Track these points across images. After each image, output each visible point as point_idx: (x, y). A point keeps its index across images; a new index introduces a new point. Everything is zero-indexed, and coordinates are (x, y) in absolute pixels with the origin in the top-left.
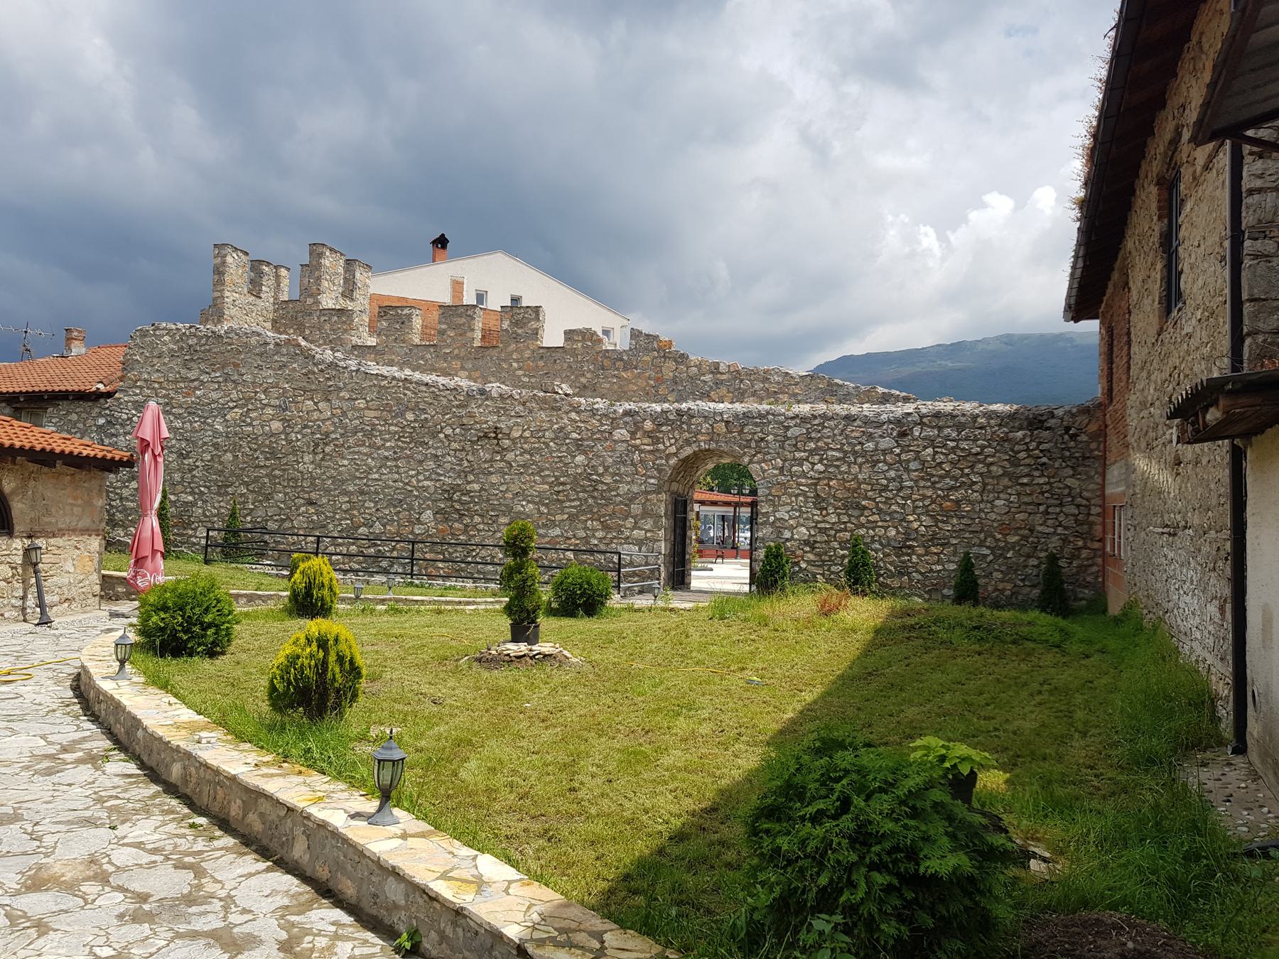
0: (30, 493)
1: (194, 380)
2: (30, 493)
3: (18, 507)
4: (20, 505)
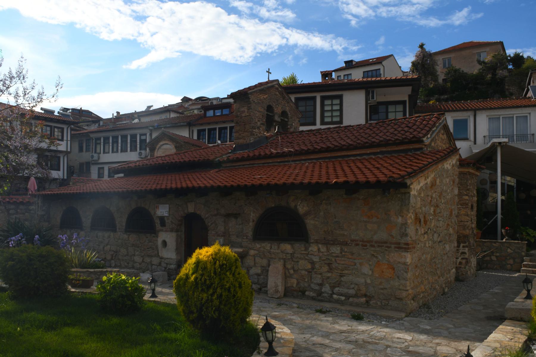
0: (322, 213)
2: (322, 213)
3: (310, 223)
4: (312, 222)
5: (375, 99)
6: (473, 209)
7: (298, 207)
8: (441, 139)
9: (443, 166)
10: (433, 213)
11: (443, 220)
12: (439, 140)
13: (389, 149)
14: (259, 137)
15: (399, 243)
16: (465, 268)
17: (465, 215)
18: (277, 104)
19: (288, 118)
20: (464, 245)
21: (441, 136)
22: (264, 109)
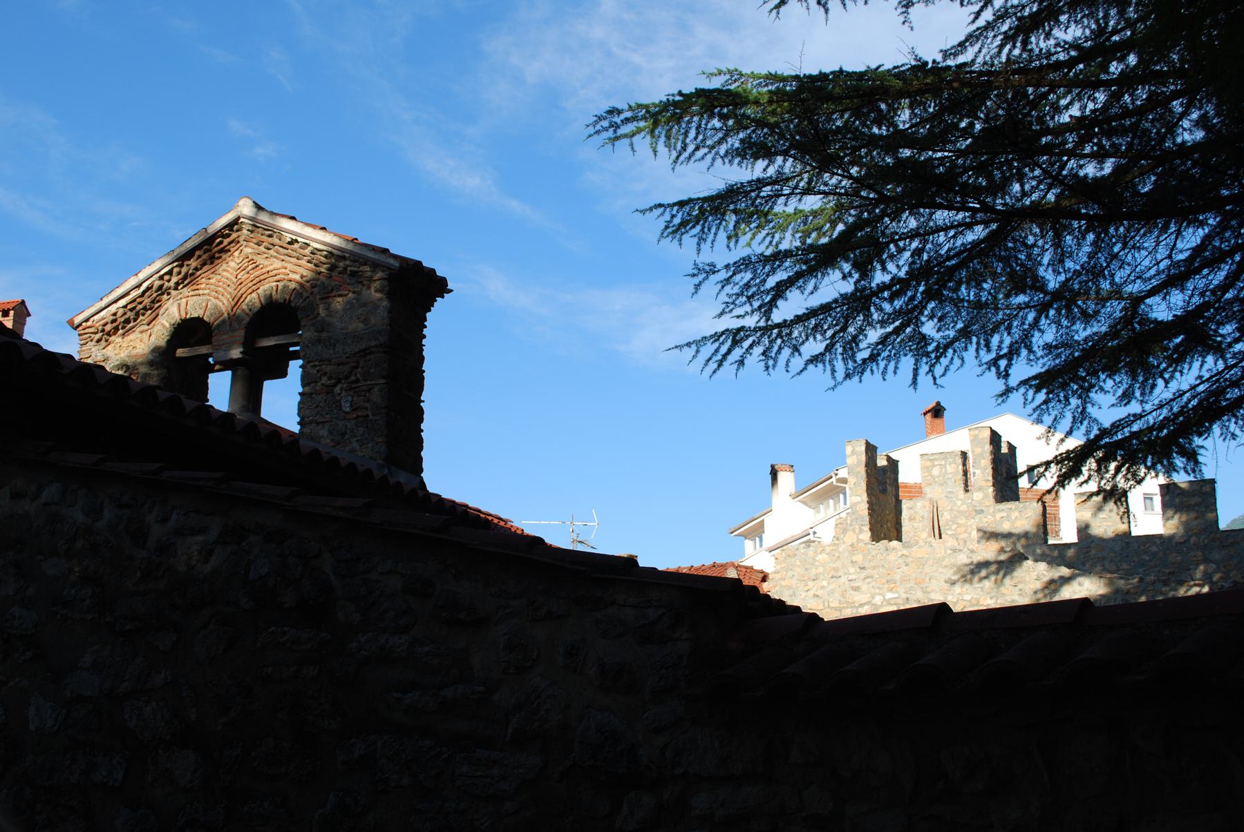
1: (865, 604)
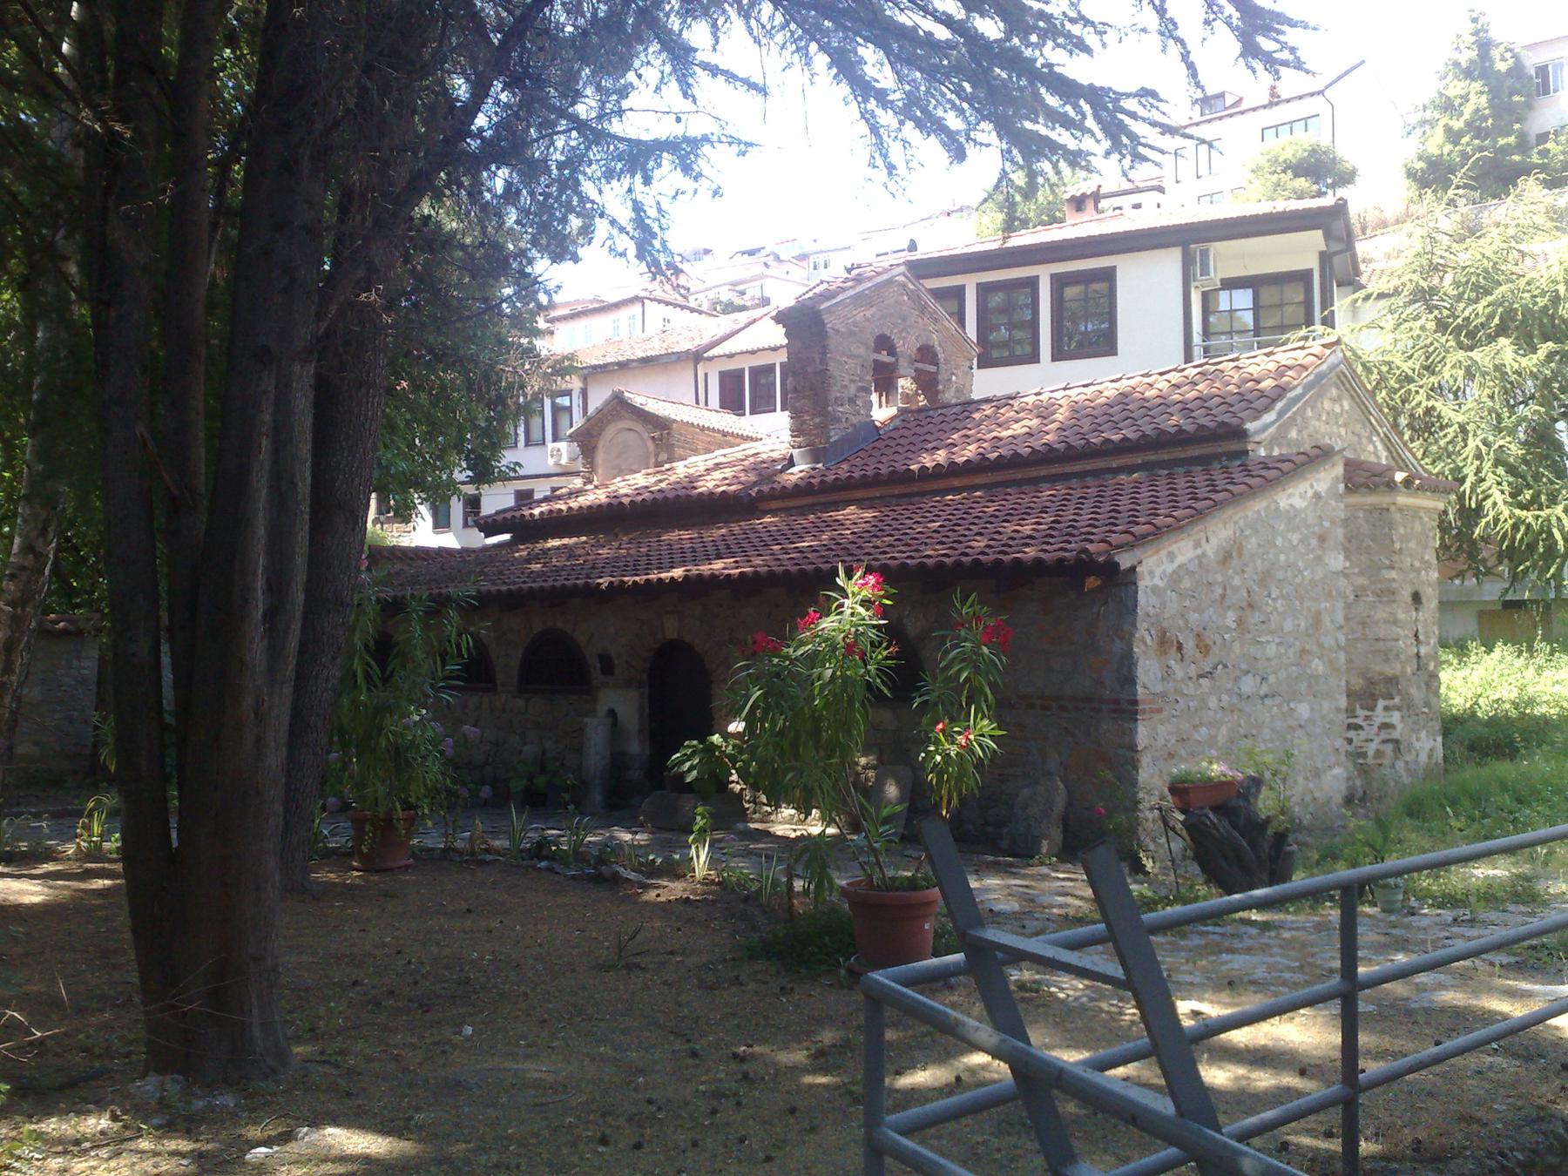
5: (1212, 274)
6: (1421, 603)
7: (905, 620)
8: (1328, 413)
9: (1273, 507)
10: (1234, 626)
11: (1277, 640)
12: (1319, 419)
13: (1166, 457)
14: (853, 425)
15: (1117, 701)
16: (1393, 766)
17: (1389, 622)
18: (904, 329)
19: (937, 364)
20: (1388, 703)
21: (1327, 404)
22: (867, 348)
